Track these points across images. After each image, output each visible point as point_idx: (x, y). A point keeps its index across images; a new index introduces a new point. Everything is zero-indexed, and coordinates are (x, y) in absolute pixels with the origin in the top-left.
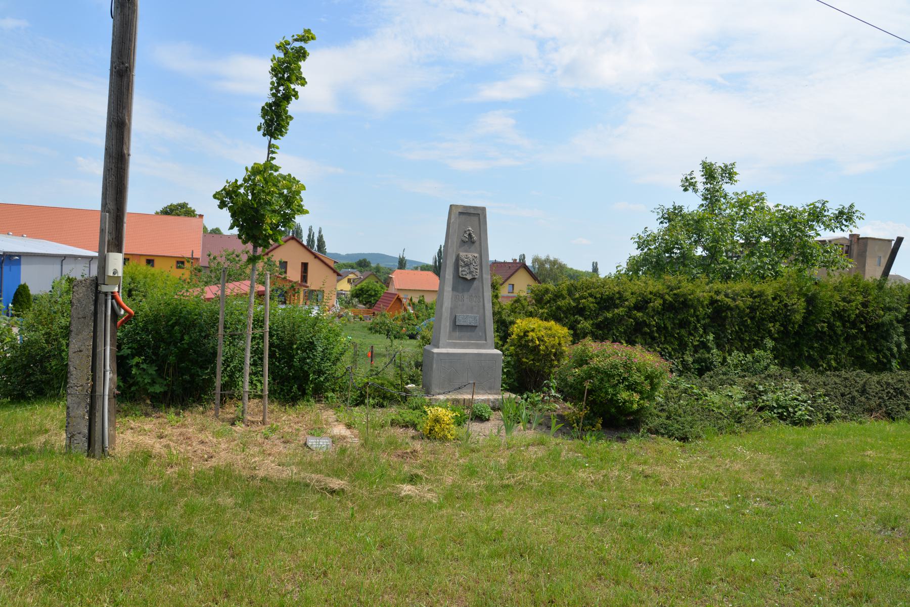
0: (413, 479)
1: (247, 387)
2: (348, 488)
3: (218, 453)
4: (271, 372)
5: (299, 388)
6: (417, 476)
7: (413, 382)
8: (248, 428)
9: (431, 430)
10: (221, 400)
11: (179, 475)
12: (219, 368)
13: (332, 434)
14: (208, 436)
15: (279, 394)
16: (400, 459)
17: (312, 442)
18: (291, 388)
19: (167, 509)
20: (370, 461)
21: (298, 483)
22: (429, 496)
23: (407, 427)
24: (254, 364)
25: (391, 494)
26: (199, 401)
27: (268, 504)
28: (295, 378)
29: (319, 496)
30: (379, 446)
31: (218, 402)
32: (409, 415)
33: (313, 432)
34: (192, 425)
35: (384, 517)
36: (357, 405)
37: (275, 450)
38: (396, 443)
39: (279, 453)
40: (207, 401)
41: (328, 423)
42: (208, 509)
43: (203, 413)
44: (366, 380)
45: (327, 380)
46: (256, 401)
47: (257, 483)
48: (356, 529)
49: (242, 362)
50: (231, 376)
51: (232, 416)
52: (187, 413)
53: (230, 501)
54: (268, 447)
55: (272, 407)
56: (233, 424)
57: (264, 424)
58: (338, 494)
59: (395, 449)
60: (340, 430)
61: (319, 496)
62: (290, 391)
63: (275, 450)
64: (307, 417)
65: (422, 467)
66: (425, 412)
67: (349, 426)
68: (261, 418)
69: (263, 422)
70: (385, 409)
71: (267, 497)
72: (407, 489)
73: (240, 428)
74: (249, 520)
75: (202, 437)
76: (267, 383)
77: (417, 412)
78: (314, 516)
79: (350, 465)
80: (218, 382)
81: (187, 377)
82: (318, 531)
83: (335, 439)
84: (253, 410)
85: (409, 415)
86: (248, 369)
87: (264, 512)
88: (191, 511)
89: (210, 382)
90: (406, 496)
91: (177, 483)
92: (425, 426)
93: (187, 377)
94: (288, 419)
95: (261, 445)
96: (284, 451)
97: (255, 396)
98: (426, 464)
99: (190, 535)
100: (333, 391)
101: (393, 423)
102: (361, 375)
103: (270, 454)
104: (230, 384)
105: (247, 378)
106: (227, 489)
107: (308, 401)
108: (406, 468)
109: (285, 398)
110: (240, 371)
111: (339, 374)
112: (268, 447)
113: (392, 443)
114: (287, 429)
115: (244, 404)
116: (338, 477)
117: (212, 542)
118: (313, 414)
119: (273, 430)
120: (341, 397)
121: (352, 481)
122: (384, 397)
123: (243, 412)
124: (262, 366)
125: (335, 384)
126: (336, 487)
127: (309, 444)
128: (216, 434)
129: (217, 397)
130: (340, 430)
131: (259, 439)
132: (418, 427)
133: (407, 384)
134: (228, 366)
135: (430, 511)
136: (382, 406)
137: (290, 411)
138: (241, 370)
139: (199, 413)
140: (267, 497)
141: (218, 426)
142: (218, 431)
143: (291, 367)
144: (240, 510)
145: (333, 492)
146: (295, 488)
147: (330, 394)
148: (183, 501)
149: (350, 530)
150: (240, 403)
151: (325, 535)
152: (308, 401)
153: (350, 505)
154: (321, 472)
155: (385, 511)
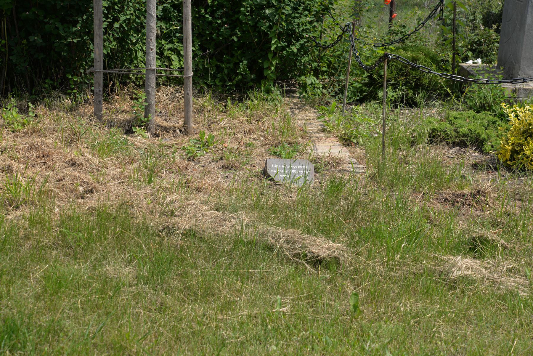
0: (475, 247)
1: (154, 63)
2: (347, 257)
3: (104, 184)
4: (197, 35)
5: (250, 67)
6: (484, 240)
7: (478, 54)
8: (158, 140)
9: (514, 152)
10: (106, 86)
11: (32, 222)
12: (99, 24)
13: (314, 155)
14: (83, 152)
15: (214, 77)
16: (449, 207)
17: (276, 167)
18: (237, 65)
19: (10, 282)
20: (388, 208)
21: (251, 243)
22: (510, 282)
23: (462, 144)
24: (164, 17)
25: (431, 273)
26: (64, 87)
27: (196, 279)
28: (244, 46)
29: (292, 268)
30: (405, 180)
31: (99, 88)
32: (467, 122)
33: (278, 150)
34: (53, 131)
35: (417, 315)
36: (361, 101)
37: (208, 181)
38: (441, 176)
39: (217, 188)
40: (80, 87)
41: (305, 134)
42: (87, 285)
43: (72, 110)
44: (381, 52)
45: (303, 50)
46: (171, 89)
47: (177, 240)
48: (362, 334)
49: (143, 13)
50: (122, 40)
51: (128, 117)
52: (41, 110)
53: (127, 273)
54: (196, 175)
55: (201, 102)
56: (129, 132)
57: (187, 133)
58: (327, 266)
59: (440, 186)
60: (329, 148)
61: (292, 268)
62: (234, 71)
63: (208, 181)
64: (267, 122)
65: (495, 224)
66: (503, 116)
67: (347, 141)
68: (181, 123)
69: (185, 130)
70: (415, 110)
71: (195, 266)
72: (463, 265)
73: (141, 139)
74: (162, 308)
75: (72, 153)
76: (190, 54)
77: (487, 116)
78: (283, 306)
79: (350, 213)
80: (98, 51)
81: (37, 39)
82: (291, 334)
83: (319, 165)
84: (165, 106)
85: (467, 122)
86: (153, 27)
87: (190, 293)
88: (55, 286)
89: (82, 50)
90: (463, 279)
91: (27, 237)
92: (501, 142)
93: (37, 39)
94: (231, 124)
95: (182, 171)
96: (226, 184)
97: (171, 81)
98: (505, 219)
99: (55, 331)
100: (317, 73)
101: (434, 137)
102: (372, 39)
103: (199, 189)
104: (121, 56)
105: (154, 44)
106: (122, 249)
107: (268, 91)
108: (461, 225)
109: (224, 85)
110: (138, 31)
111: (327, 39)
112: (196, 175)
113: (432, 175)
114: (229, 143)
115: (148, 94)
116: (328, 235)
117: (95, 345)
118: (278, 117)
119: (205, 145)
120: (332, 84)
121: (353, 244)
122: (417, 87)
123: (147, 110)
124: (181, 21)
125: (321, 58)
126: (324, 254)
127: (272, 172)
128: (99, 149)
129: (98, 80)
130: (329, 148)
131: (179, 160)
132: (487, 146)
133: (466, 59)
134: (116, 19)
135: (513, 311)
136: (412, 104)
137: (235, 110)
138: (140, 28)
139: (65, 110)
140: (195, 266)
141: (102, 134)
142: (102, 145)
143: (235, 24)
144: (147, 288)
145: (317, 262)
146: (249, 251)
147: (310, 80)
148: (39, 271)
149: (352, 335)
150: (141, 94)
151: (304, 341)
152: (268, 91)
153: (350, 288)
154: (294, 224)
155: (420, 305)
